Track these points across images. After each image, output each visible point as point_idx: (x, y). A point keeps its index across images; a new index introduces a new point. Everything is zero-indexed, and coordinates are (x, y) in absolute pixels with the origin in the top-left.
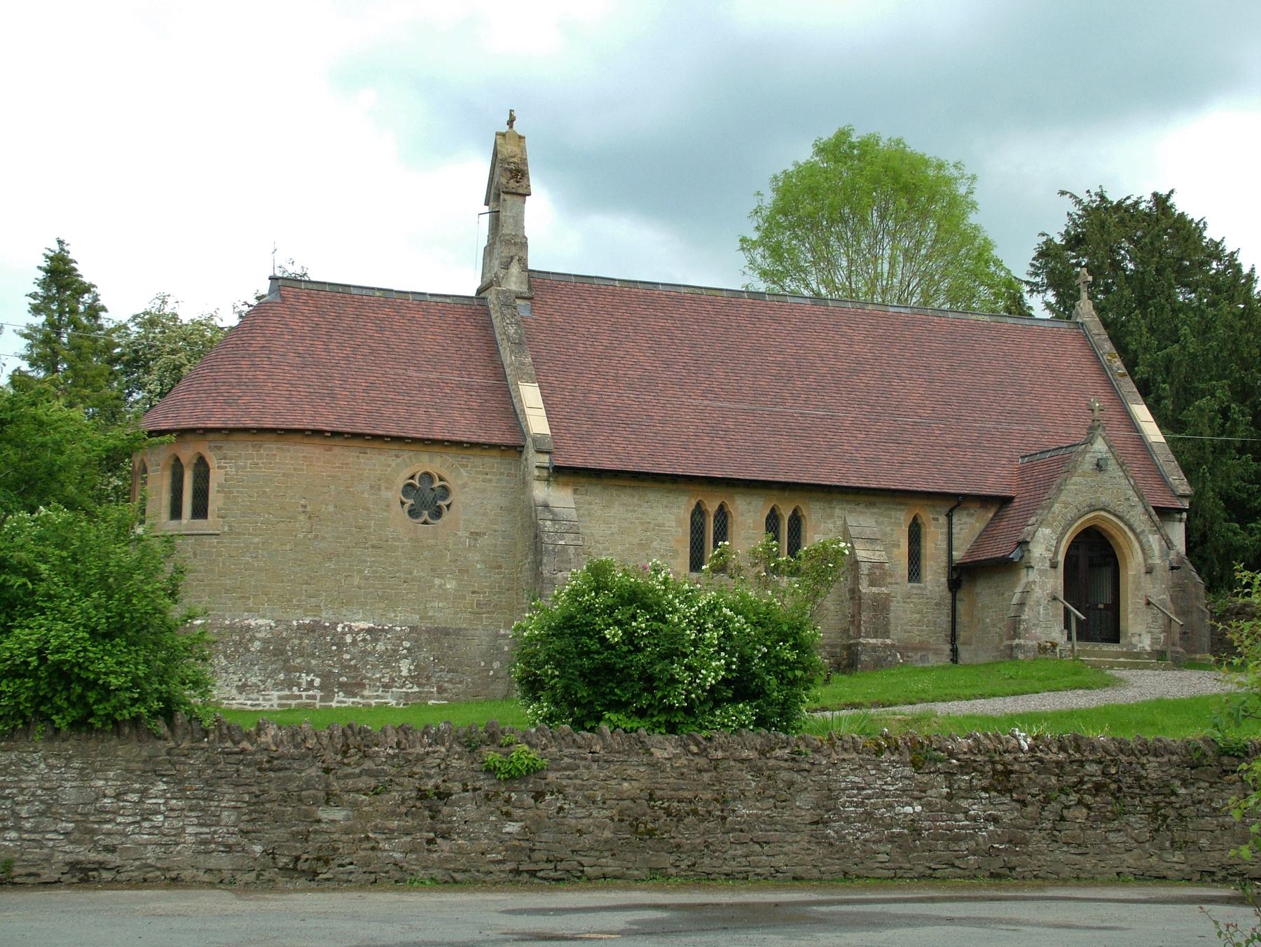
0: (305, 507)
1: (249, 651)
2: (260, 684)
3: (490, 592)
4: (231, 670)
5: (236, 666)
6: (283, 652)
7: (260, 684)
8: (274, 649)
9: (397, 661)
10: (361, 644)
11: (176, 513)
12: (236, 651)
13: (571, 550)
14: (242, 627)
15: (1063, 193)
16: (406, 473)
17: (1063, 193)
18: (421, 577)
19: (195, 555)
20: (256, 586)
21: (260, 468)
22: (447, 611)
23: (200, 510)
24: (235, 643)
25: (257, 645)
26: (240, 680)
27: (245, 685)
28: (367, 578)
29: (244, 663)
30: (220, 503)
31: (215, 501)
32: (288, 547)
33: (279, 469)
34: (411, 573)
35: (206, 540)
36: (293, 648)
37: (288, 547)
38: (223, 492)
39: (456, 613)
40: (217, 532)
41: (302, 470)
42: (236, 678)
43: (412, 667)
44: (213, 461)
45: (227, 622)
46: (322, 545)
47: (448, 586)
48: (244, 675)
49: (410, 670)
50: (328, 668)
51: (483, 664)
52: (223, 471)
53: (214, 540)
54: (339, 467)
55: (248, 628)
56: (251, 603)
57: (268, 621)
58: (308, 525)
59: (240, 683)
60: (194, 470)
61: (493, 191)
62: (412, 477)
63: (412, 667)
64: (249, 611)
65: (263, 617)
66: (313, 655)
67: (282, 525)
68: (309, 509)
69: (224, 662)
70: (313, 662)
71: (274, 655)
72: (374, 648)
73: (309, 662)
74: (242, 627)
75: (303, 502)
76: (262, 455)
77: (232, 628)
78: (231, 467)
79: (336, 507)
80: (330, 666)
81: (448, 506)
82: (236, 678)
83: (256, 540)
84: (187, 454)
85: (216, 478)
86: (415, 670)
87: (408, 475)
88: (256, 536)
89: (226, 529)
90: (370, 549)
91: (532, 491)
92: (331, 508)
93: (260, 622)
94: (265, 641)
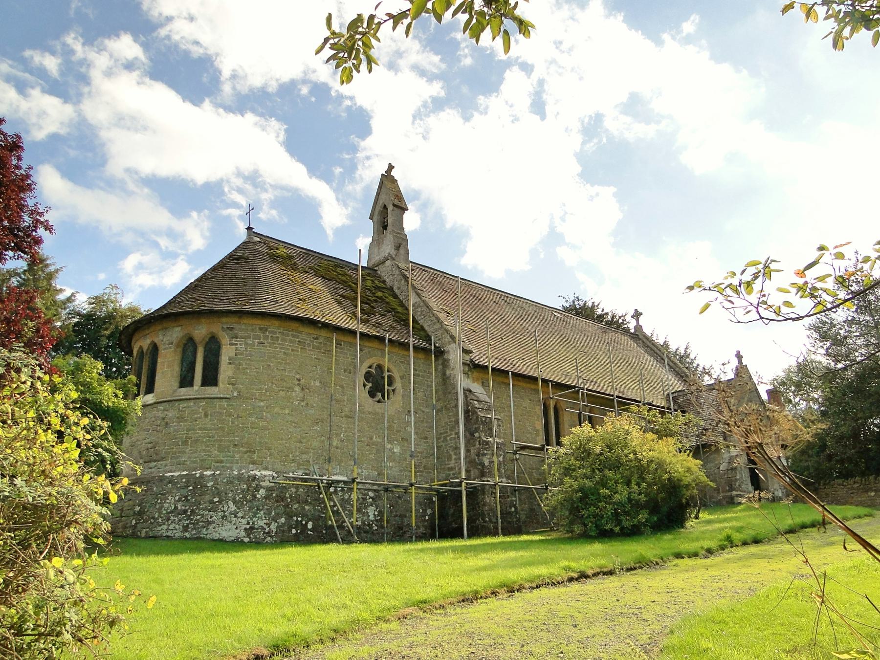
0: (299, 380)
1: (256, 497)
2: (265, 526)
3: (421, 456)
4: (240, 515)
5: (244, 511)
6: (283, 499)
7: (265, 526)
8: (277, 496)
9: (366, 508)
10: (340, 493)
11: (186, 381)
12: (244, 497)
13: (495, 422)
14: (249, 477)
15: (691, 288)
16: (366, 364)
17: (691, 288)
18: (378, 442)
19: (206, 415)
20: (260, 442)
21: (266, 347)
22: (394, 469)
23: (211, 379)
24: (243, 491)
25: (262, 492)
26: (248, 523)
27: (252, 528)
28: (342, 441)
29: (251, 508)
30: (230, 373)
31: (225, 371)
32: (287, 411)
33: (281, 348)
34: (372, 439)
35: (217, 403)
36: (291, 496)
37: (287, 411)
38: (234, 363)
39: (401, 471)
40: (228, 396)
41: (298, 351)
42: (244, 521)
43: (376, 513)
44: (225, 340)
45: (236, 473)
46: (312, 411)
47: (395, 451)
48: (251, 519)
49: (375, 515)
50: (317, 514)
51: (421, 511)
52: (234, 347)
53: (225, 403)
54: (323, 353)
55: (254, 478)
56: (255, 457)
57: (270, 473)
58: (301, 395)
59: (248, 527)
60: (205, 348)
61: (378, 209)
62: (370, 367)
63: (376, 513)
64: (253, 463)
65: (266, 469)
66: (306, 502)
67: (282, 393)
68: (302, 382)
69: (233, 507)
70: (307, 508)
71: (277, 501)
72: (350, 496)
73: (303, 508)
74: (249, 477)
75: (298, 376)
76: (268, 336)
77: (240, 478)
78: (240, 344)
79: (320, 382)
80: (319, 511)
81: (393, 391)
82: (244, 521)
83: (262, 404)
84: (201, 331)
85: (227, 353)
86: (378, 515)
87: (368, 365)
88: (262, 401)
89: (235, 394)
90: (344, 418)
91: (43, 139)
92: (318, 384)
93: (264, 473)
94: (269, 489)
